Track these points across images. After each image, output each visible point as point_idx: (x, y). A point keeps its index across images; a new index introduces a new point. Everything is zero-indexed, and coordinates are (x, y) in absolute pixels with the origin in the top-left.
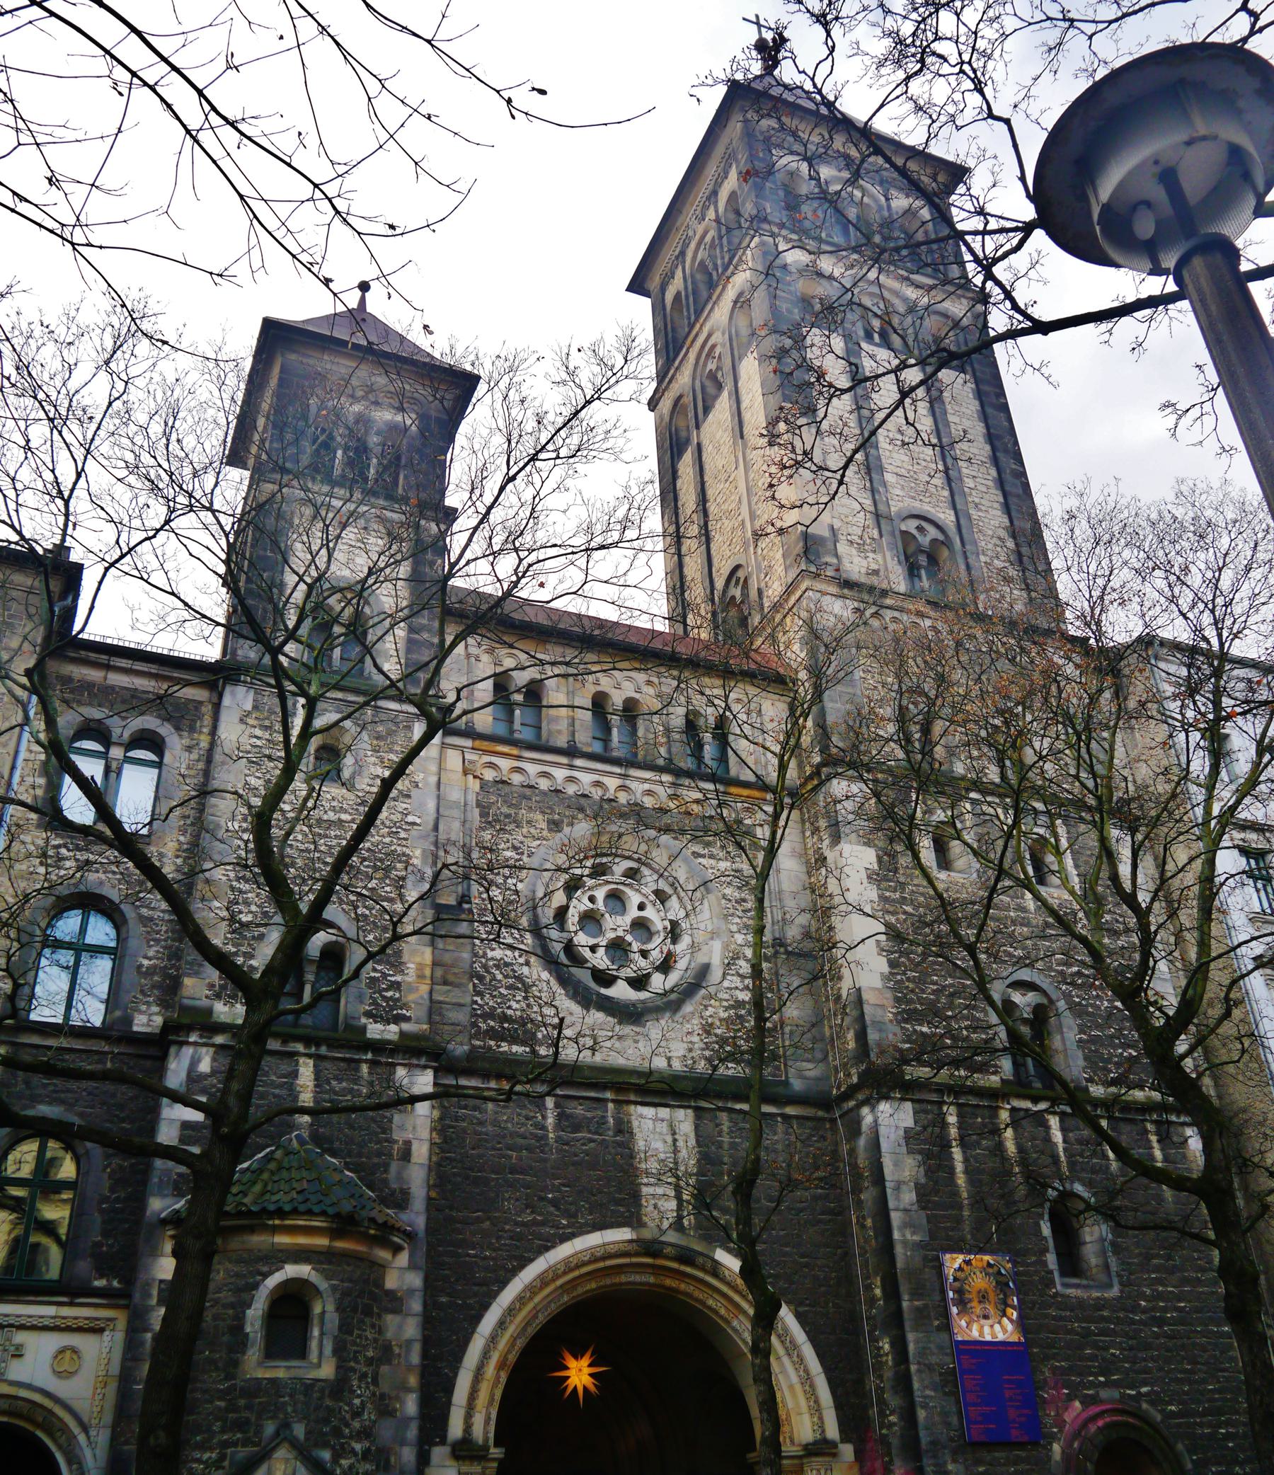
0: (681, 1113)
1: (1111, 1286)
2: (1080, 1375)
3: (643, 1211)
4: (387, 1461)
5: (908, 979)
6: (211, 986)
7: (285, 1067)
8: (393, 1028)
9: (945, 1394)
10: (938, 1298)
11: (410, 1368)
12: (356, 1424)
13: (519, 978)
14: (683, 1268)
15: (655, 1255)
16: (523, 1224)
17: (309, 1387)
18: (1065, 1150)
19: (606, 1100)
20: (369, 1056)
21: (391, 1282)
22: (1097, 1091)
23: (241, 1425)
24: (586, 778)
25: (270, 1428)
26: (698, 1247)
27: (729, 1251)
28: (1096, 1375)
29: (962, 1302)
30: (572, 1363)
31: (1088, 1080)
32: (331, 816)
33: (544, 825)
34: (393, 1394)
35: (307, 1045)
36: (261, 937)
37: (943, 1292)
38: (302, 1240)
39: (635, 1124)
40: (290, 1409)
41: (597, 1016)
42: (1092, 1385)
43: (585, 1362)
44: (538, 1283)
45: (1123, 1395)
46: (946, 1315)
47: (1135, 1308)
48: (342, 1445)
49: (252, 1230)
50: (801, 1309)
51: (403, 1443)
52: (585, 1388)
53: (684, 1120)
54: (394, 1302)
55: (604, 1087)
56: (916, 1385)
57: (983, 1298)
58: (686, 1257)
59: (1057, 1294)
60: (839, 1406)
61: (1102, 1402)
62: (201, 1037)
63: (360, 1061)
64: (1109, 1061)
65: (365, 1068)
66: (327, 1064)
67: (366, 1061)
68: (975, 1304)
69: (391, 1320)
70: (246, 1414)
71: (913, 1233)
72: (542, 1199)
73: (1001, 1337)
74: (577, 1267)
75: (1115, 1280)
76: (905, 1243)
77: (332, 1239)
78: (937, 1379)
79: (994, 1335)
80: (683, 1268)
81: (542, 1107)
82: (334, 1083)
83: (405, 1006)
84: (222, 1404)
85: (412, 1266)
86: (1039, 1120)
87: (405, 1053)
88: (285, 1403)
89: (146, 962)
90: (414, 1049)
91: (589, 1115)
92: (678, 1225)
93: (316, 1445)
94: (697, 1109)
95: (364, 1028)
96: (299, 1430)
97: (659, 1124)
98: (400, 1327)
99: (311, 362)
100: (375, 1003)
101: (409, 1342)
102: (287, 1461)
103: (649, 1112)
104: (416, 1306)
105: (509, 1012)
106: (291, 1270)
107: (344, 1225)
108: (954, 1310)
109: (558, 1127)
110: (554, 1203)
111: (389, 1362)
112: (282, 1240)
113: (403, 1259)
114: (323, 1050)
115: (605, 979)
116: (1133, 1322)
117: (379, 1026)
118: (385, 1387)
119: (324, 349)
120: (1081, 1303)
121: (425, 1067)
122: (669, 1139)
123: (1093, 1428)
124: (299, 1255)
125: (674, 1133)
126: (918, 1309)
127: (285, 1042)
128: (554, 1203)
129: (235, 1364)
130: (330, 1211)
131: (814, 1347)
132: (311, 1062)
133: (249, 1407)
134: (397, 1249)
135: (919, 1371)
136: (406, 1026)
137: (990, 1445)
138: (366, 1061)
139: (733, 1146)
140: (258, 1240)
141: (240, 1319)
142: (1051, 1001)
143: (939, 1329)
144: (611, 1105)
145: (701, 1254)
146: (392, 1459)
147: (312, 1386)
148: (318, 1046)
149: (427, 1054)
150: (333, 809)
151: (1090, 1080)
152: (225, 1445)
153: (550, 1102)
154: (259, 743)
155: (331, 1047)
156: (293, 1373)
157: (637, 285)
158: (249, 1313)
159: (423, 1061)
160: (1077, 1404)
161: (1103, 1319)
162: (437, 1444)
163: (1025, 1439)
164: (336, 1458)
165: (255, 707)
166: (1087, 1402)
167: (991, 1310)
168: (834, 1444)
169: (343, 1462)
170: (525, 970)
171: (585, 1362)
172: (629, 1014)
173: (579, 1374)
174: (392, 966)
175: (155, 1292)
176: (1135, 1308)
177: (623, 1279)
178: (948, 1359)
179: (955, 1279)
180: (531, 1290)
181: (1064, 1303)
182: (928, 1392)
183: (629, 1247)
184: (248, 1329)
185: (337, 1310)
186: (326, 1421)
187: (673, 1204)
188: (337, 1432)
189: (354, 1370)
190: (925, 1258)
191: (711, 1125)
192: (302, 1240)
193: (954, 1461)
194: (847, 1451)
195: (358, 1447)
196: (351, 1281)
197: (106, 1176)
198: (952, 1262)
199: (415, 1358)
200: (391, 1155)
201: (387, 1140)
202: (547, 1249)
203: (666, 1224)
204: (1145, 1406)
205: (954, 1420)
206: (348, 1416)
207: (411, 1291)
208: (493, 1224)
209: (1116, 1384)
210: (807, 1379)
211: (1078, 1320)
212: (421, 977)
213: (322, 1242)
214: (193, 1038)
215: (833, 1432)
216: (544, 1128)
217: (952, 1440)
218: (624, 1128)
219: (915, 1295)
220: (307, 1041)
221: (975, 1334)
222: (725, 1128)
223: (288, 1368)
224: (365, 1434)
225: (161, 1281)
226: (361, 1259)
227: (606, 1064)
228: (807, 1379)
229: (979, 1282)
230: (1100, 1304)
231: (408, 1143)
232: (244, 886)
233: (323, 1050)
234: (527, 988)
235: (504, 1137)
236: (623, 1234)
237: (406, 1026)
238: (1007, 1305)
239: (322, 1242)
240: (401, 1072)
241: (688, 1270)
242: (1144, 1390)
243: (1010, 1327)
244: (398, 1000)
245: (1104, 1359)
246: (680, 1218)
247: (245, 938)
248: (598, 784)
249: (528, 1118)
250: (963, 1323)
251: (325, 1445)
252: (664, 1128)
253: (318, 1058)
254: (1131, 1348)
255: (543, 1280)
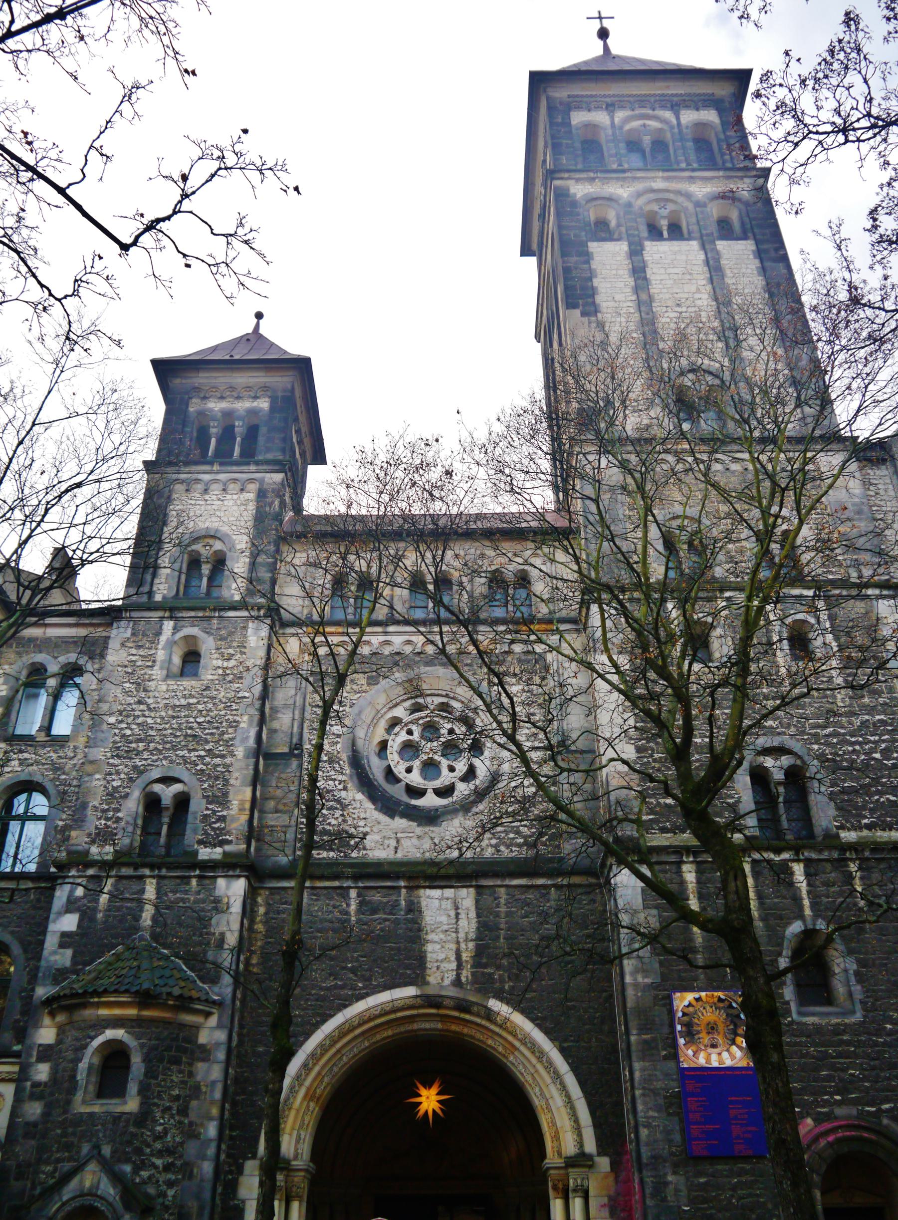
0: (464, 892)
1: (853, 1012)
2: (812, 1094)
3: (428, 972)
4: (192, 1172)
5: (655, 761)
6: (89, 835)
7: (135, 887)
8: (219, 850)
9: (669, 1114)
10: (666, 1030)
11: (212, 1102)
12: (158, 1145)
13: (338, 801)
14: (463, 1016)
15: (438, 1006)
16: (327, 989)
17: (117, 1118)
18: (809, 892)
19: (399, 888)
20: (197, 872)
21: (203, 1038)
22: (849, 836)
23: (68, 1147)
24: (397, 640)
25: (85, 1149)
26: (472, 998)
27: (501, 1000)
28: (831, 1094)
29: (690, 1034)
30: (424, 1092)
31: (838, 828)
32: (183, 702)
33: (364, 681)
34: (198, 1121)
35: (152, 869)
36: (127, 795)
37: (672, 1026)
38: (117, 1012)
39: (423, 904)
40: (101, 1135)
41: (400, 823)
42: (826, 1103)
43: (434, 1091)
44: (337, 1033)
45: (861, 1113)
46: (675, 1045)
47: (880, 1031)
48: (143, 1161)
49: (84, 1006)
50: (565, 1045)
51: (204, 1158)
52: (426, 1112)
53: (467, 897)
54: (205, 1053)
55: (398, 877)
56: (640, 1107)
57: (712, 1028)
58: (463, 1006)
59: (792, 1022)
60: (597, 1125)
61: (836, 1118)
62: (78, 871)
63: (190, 877)
64: (864, 807)
65: (194, 882)
66: (166, 882)
67: (195, 877)
68: (703, 1035)
69: (201, 1067)
70: (72, 1139)
71: (644, 977)
72: (345, 968)
73: (728, 1063)
74: (370, 1019)
75: (858, 1007)
76: (636, 985)
77: (140, 1010)
78: (661, 1101)
79: (721, 1061)
80: (463, 1016)
81: (346, 897)
82: (170, 895)
83: (229, 833)
84: (59, 1131)
85: (220, 1026)
86: (784, 870)
87: (223, 867)
88: (98, 1130)
89: (61, 823)
90: (230, 866)
91: (385, 900)
92: (457, 982)
93: (119, 1161)
94: (478, 888)
95: (196, 853)
96: (107, 1150)
97: (444, 903)
98: (208, 1072)
99: (189, 381)
100: (206, 833)
101: (214, 1083)
102: (94, 1172)
103: (436, 893)
104: (221, 1055)
105: (328, 827)
106: (110, 1034)
107: (145, 999)
108: (682, 1041)
109: (359, 911)
110: (353, 971)
111: (197, 1098)
112: (103, 1012)
113: (213, 1021)
114: (164, 872)
115: (415, 792)
116: (876, 1044)
117: (208, 850)
118: (193, 1116)
119: (198, 370)
120: (818, 1029)
121: (239, 876)
122: (452, 913)
123: (823, 1143)
124: (117, 1023)
125: (457, 908)
126: (645, 1042)
127: (136, 869)
128: (353, 971)
129: (69, 1102)
130: (134, 989)
131: (576, 1075)
132: (154, 881)
133: (74, 1134)
134: (208, 1015)
135: (643, 1095)
136: (228, 848)
137: (713, 1158)
138: (195, 877)
139: (508, 914)
140: (88, 1013)
141: (74, 1070)
142: (804, 762)
143: (665, 1058)
144: (404, 891)
145: (477, 1004)
146: (195, 1170)
147: (120, 1117)
148: (159, 869)
149: (240, 866)
150: (184, 697)
151: (842, 827)
152: (58, 1161)
153: (353, 893)
154: (134, 658)
155: (169, 869)
156: (104, 1109)
157: (526, 251)
158: (80, 1065)
159: (237, 872)
160: (809, 1121)
161: (842, 1043)
162: (249, 1159)
163: (750, 1153)
164: (136, 1170)
165: (133, 634)
166: (819, 1119)
167: (720, 1039)
168: (590, 1157)
169: (142, 1173)
170: (343, 794)
171: (434, 1091)
172: (430, 818)
173: (429, 1100)
174: (221, 804)
175: (35, 1053)
176: (880, 1031)
177: (415, 1026)
178: (675, 1084)
179: (684, 1014)
180: (332, 1039)
181: (802, 1030)
182: (651, 1113)
183: (419, 1000)
184: (79, 1078)
185: (144, 1061)
186: (129, 1143)
187: (454, 965)
188: (139, 1151)
189: (157, 1106)
190: (655, 997)
191: (491, 899)
192: (117, 1012)
193: (675, 1173)
194: (604, 1163)
195: (159, 1162)
196: (158, 1039)
197: (25, 973)
198: (683, 1000)
199: (218, 1095)
200: (208, 944)
201: (207, 934)
202: (346, 1006)
203: (447, 982)
204: (885, 1121)
205: (677, 1137)
206: (149, 1139)
207: (218, 1044)
208: (303, 990)
209: (855, 1102)
210: (569, 1102)
211: (814, 1044)
212: (241, 810)
213: (132, 1012)
214: (73, 872)
215: (590, 1146)
216: (347, 913)
217: (672, 1154)
218: (414, 909)
219: (642, 1029)
220: (152, 867)
221: (702, 1061)
222: (502, 901)
223: (103, 1104)
224: (168, 1151)
225: (40, 1045)
226: (170, 1023)
227: (405, 859)
228: (569, 1102)
229: (709, 1015)
230: (837, 1030)
231: (222, 935)
232: (116, 761)
233: (164, 872)
234: (344, 807)
235: (315, 923)
236: (410, 991)
237: (228, 848)
238: (736, 1034)
239: (132, 1012)
240: (221, 882)
241: (467, 1017)
242: (886, 1106)
243: (738, 1054)
244: (223, 829)
245: (841, 1080)
246: (458, 975)
247: (115, 798)
248: (409, 642)
249: (334, 907)
250: (690, 1052)
251: (127, 1161)
252: (448, 905)
253: (160, 878)
254: (873, 1068)
255: (342, 1031)
